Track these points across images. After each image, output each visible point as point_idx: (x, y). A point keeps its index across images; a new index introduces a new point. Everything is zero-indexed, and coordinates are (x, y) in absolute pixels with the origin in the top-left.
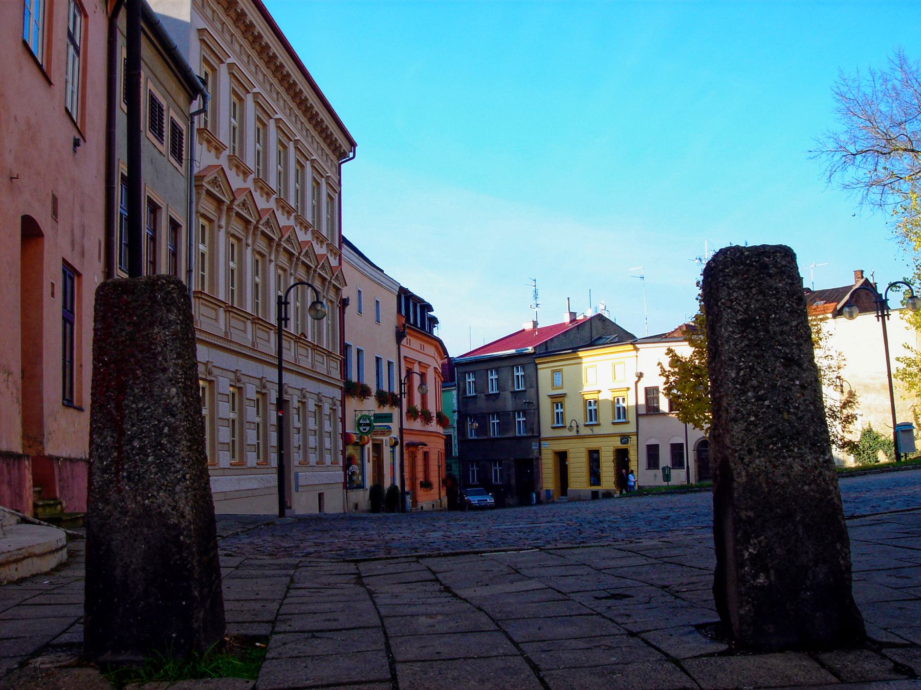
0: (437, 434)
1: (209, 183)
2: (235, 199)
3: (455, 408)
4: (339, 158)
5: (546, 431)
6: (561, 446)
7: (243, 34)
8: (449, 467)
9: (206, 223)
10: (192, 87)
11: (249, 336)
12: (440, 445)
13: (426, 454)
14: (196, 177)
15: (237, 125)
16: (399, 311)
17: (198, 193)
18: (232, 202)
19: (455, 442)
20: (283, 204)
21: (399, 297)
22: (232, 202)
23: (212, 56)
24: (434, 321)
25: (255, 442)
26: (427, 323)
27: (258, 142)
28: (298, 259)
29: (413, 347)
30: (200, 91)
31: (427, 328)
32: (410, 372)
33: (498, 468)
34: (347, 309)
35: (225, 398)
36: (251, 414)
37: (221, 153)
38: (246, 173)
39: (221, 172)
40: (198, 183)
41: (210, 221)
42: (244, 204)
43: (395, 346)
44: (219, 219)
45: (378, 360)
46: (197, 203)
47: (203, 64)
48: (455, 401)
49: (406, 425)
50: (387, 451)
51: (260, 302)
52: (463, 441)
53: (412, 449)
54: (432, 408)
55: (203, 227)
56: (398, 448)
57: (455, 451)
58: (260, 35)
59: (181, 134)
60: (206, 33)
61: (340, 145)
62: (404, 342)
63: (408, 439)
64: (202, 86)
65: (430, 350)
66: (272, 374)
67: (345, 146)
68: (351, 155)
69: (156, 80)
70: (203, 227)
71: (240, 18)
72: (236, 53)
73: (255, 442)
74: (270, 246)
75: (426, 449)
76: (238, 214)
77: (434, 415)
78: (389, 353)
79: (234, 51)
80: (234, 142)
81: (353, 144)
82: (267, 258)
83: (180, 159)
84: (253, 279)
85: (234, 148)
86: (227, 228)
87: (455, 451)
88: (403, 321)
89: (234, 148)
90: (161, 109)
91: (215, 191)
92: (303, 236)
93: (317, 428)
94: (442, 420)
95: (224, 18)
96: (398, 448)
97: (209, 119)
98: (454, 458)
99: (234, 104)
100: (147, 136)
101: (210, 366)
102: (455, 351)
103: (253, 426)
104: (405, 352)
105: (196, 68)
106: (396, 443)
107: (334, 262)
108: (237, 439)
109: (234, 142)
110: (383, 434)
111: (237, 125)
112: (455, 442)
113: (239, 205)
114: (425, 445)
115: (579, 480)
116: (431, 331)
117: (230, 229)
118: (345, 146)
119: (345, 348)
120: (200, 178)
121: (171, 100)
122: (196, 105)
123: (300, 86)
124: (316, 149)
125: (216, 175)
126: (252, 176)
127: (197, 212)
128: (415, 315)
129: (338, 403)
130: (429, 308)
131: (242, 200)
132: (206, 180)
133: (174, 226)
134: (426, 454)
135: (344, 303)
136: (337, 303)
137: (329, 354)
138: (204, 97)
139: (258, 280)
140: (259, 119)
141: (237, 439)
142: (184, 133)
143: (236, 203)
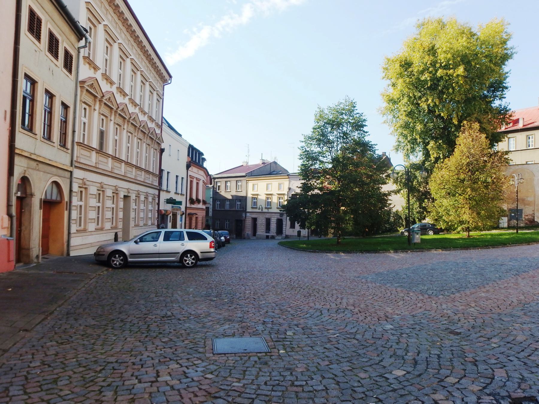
0: (202, 209)
1: (88, 86)
2: (118, 107)
3: (212, 196)
4: (163, 83)
5: (249, 209)
6: (254, 216)
7: (118, 17)
8: (207, 221)
9: (104, 118)
10: (79, 33)
11: (143, 177)
12: (204, 213)
13: (197, 218)
14: (80, 82)
15: (133, 85)
16: (189, 155)
17: (82, 91)
18: (117, 109)
19: (211, 210)
20: (151, 118)
21: (189, 149)
22: (117, 109)
23: (94, 18)
24: (204, 160)
25: (110, 217)
26: (201, 161)
27: (120, 69)
28: (139, 129)
29: (194, 171)
30: (84, 36)
31: (201, 163)
32: (191, 182)
33: (218, 222)
34: (164, 154)
35: (94, 196)
36: (109, 204)
37: (97, 71)
38: (112, 83)
39: (96, 81)
40: (82, 85)
41: (106, 117)
42: (109, 99)
43: (186, 171)
44: (95, 105)
45: (177, 176)
46: (81, 96)
47: (88, 21)
48: (212, 193)
49: (188, 205)
50: (179, 217)
51: (139, 159)
52: (214, 210)
53: (191, 216)
54: (200, 197)
55: (103, 120)
56: (184, 216)
57: (211, 214)
58: (144, 46)
59: (71, 57)
60: (90, 5)
61: (163, 75)
62: (190, 169)
63: (188, 211)
64: (85, 32)
65: (202, 173)
66: (156, 192)
67: (167, 77)
68: (170, 82)
69: (53, 23)
70: (103, 120)
71: (117, 7)
72: (108, 19)
73: (75, 218)
74: (111, 112)
75: (197, 216)
76: (120, 115)
77: (202, 201)
78: (182, 172)
79: (121, 37)
80: (106, 67)
81: (171, 77)
82: (122, 127)
83: (70, 71)
84: (136, 150)
85: (120, 83)
86: (99, 111)
87: (211, 214)
88: (190, 160)
89: (120, 83)
90: (57, 41)
91: (122, 114)
92: (142, 117)
93: (136, 207)
94: (204, 202)
95: (117, 21)
96: (184, 216)
97: (91, 52)
98: (210, 217)
99: (121, 63)
100: (25, 36)
101: (85, 180)
102: (213, 172)
103: (109, 209)
104: (190, 173)
105: (83, 21)
106: (183, 214)
107: (158, 131)
108: (114, 216)
109: (106, 67)
110: (177, 210)
111: (133, 85)
112: (211, 210)
113: (106, 100)
114: (197, 214)
115: (261, 230)
116: (203, 164)
117: (82, 99)
118: (167, 77)
119: (161, 171)
120: (83, 82)
121: (65, 37)
122: (83, 43)
123: (160, 68)
124: (151, 76)
125: (93, 82)
126: (128, 97)
127: (81, 101)
128: (195, 158)
129: (157, 196)
130: (202, 154)
131: (108, 97)
132: (87, 84)
133: (65, 106)
134: (197, 218)
135: (162, 151)
136: (158, 150)
137: (153, 174)
138: (86, 39)
139: (116, 138)
140: (121, 57)
141: (114, 216)
142: (74, 57)
143: (119, 109)
